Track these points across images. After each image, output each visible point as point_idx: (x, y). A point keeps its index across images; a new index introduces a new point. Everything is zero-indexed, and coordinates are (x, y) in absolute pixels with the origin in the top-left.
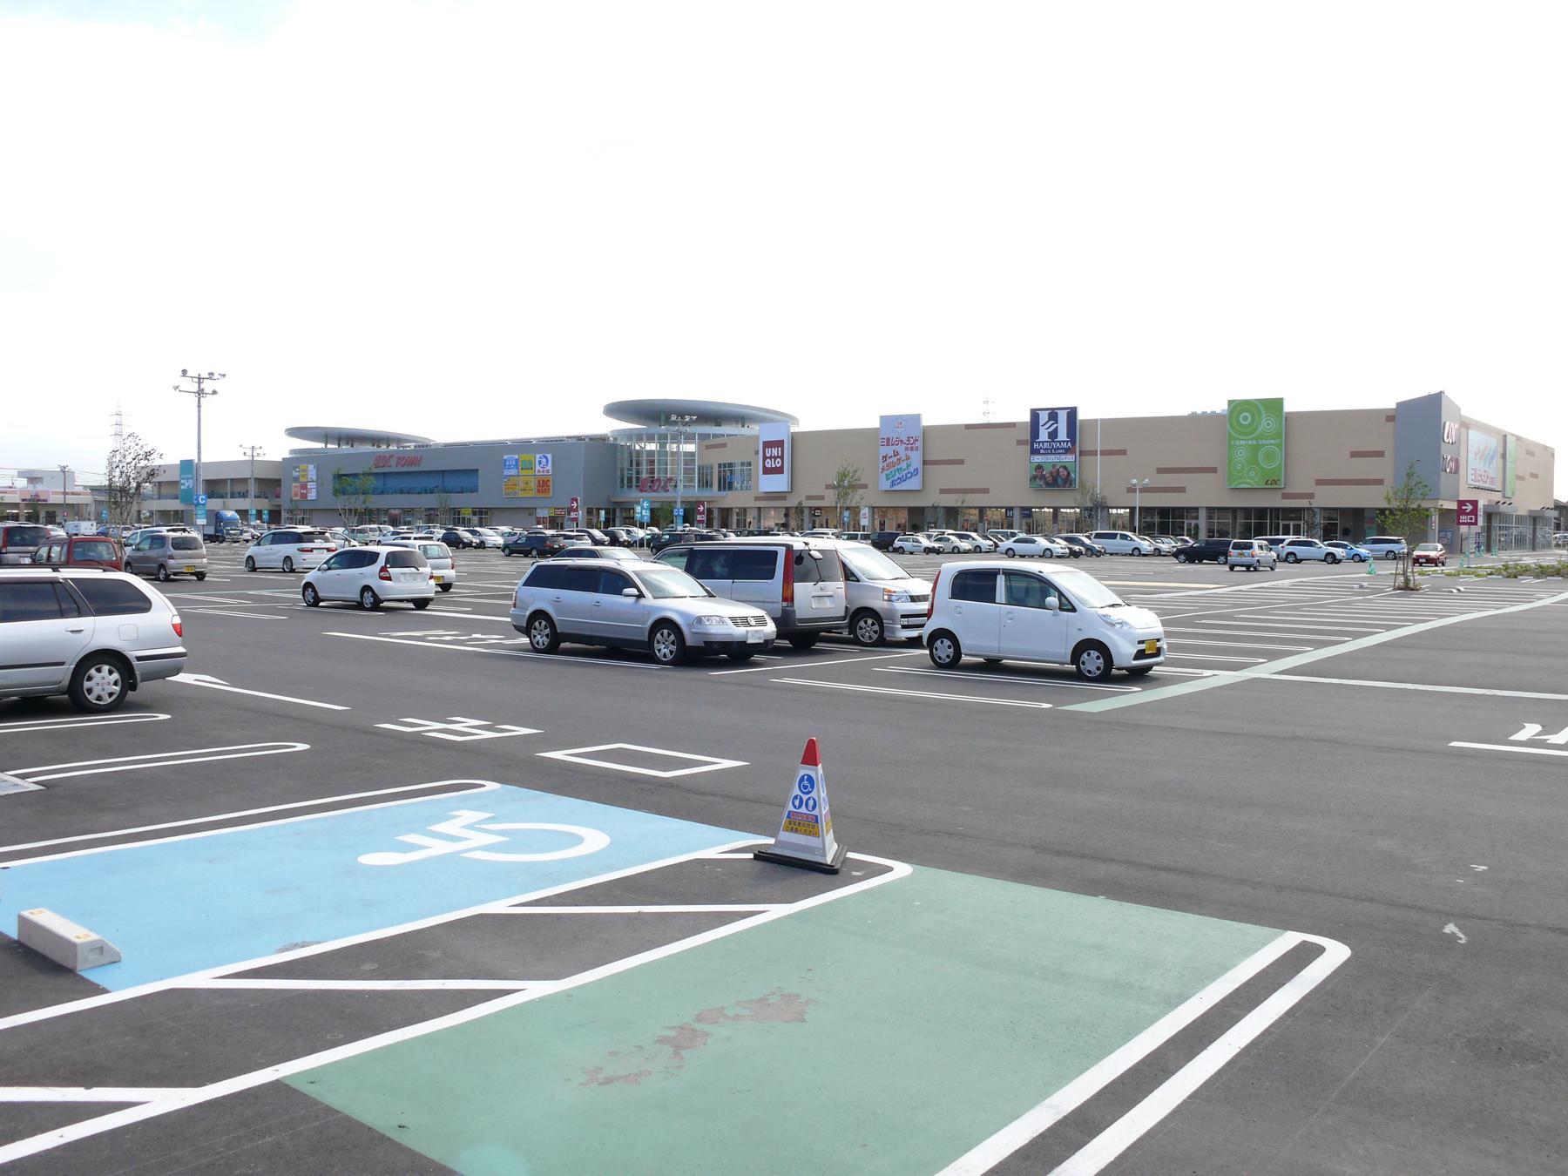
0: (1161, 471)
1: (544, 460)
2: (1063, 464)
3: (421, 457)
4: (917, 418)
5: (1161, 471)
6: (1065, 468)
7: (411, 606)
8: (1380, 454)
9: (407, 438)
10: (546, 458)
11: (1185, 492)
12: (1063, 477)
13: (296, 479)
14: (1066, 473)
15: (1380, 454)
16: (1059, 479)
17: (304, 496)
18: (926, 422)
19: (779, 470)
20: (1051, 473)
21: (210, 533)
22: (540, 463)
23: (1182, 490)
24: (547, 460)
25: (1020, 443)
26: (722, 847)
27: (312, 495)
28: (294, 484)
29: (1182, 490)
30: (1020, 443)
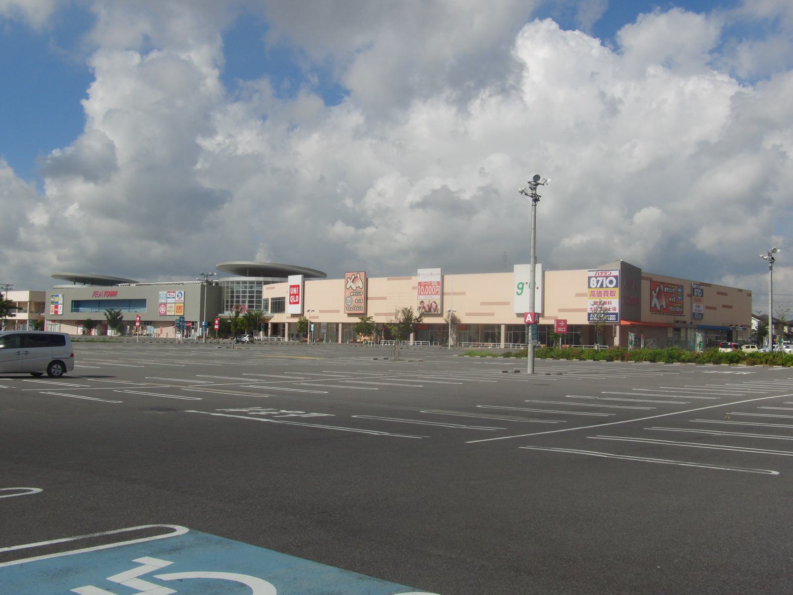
0: (482, 304)
1: (180, 294)
2: (433, 300)
3: (117, 292)
4: (388, 280)
5: (482, 304)
6: (435, 303)
7: (30, 375)
8: (338, 311)
9: (117, 280)
10: (181, 293)
11: (465, 294)
12: (434, 308)
13: (52, 303)
14: (435, 305)
15: (338, 311)
16: (432, 309)
17: (56, 312)
18: (386, 278)
19: (298, 303)
20: (428, 305)
21: (298, 313)
22: (178, 296)
23: (492, 314)
24: (182, 295)
25: (414, 288)
26: (66, 555)
27: (60, 312)
28: (51, 306)
29: (492, 314)
30: (414, 288)
